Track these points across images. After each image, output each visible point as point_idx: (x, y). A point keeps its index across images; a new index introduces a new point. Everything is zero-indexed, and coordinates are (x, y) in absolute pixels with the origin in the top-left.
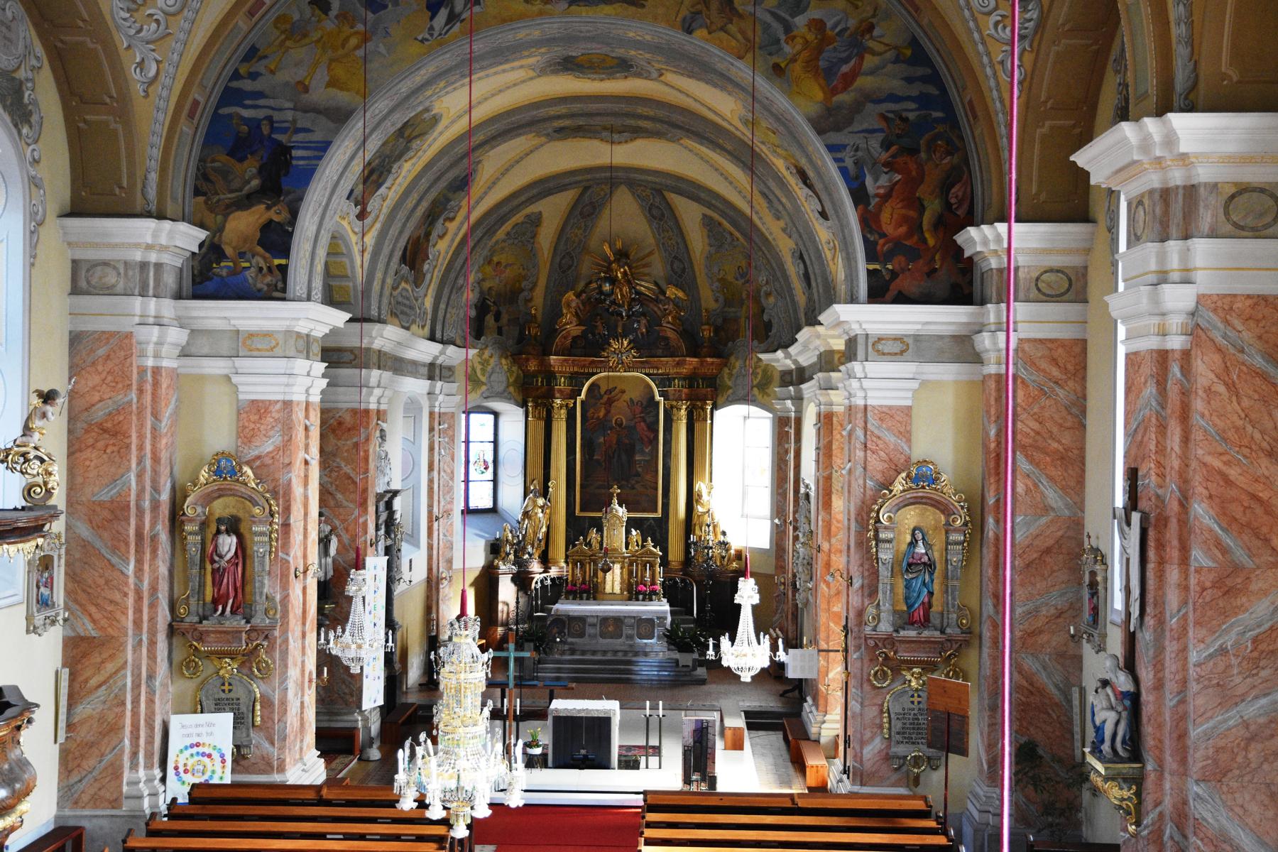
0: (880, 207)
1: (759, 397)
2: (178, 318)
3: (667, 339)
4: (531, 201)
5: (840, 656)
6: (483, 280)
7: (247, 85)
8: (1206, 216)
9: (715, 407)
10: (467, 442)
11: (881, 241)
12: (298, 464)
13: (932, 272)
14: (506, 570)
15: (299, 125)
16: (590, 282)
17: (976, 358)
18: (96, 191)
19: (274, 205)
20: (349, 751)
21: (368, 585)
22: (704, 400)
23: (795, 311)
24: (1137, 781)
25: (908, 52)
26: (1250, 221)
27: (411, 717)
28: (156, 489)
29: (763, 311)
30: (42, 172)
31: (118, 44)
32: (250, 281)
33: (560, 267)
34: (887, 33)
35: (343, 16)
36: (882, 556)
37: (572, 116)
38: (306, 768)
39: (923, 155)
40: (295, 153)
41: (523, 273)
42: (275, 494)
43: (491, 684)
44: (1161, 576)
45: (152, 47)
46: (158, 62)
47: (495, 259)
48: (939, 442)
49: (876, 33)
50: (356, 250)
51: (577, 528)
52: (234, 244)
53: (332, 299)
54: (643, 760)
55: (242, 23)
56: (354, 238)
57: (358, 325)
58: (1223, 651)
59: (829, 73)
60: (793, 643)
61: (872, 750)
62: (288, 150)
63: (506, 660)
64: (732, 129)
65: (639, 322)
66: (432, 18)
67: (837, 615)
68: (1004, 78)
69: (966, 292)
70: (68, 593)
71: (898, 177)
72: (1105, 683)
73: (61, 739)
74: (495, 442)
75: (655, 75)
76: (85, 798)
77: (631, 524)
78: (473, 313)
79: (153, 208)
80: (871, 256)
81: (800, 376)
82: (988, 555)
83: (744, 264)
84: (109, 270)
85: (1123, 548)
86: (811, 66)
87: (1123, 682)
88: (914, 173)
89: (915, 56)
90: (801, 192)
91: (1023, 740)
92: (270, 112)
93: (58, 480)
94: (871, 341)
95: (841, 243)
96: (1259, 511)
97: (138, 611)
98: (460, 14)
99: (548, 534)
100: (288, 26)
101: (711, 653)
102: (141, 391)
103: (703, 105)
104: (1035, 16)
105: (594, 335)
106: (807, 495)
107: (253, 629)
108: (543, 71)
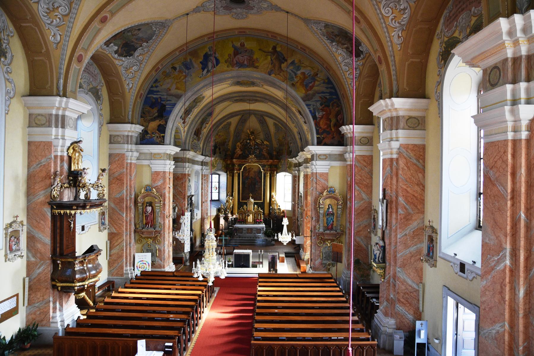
0: (320, 121)
2: (136, 150)
3: (264, 155)
4: (228, 119)
5: (309, 238)
7: (155, 89)
8: (402, 124)
9: (277, 173)
10: (212, 182)
12: (167, 188)
13: (333, 138)
14: (222, 216)
17: (345, 160)
18: (116, 117)
20: (181, 263)
21: (186, 219)
24: (384, 268)
26: (412, 126)
27: (197, 254)
28: (131, 194)
30: (102, 112)
34: (321, 76)
35: (180, 71)
36: (321, 212)
37: (239, 96)
38: (170, 267)
40: (167, 106)
42: (161, 196)
43: (218, 246)
44: (391, 216)
48: (335, 182)
49: (318, 76)
50: (182, 131)
51: (240, 205)
53: (176, 145)
54: (258, 265)
55: (154, 73)
56: (182, 129)
57: (183, 151)
58: (406, 235)
59: (306, 86)
60: (297, 235)
61: (317, 262)
62: (165, 106)
63: (222, 239)
67: (309, 227)
68: (351, 88)
70: (109, 221)
71: (324, 113)
72: (377, 244)
73: (108, 259)
74: (219, 182)
76: (115, 274)
77: (255, 203)
78: (213, 148)
79: (130, 121)
80: (318, 133)
81: (299, 165)
82: (348, 211)
84: (119, 137)
85: (382, 209)
87: (381, 243)
89: (328, 81)
90: (299, 116)
91: (356, 258)
92: (160, 96)
93: (106, 192)
95: (310, 129)
96: (415, 199)
97: (126, 226)
99: (233, 206)
101: (276, 237)
102: (127, 169)
106: (301, 196)
107: (156, 231)
108: (231, 85)
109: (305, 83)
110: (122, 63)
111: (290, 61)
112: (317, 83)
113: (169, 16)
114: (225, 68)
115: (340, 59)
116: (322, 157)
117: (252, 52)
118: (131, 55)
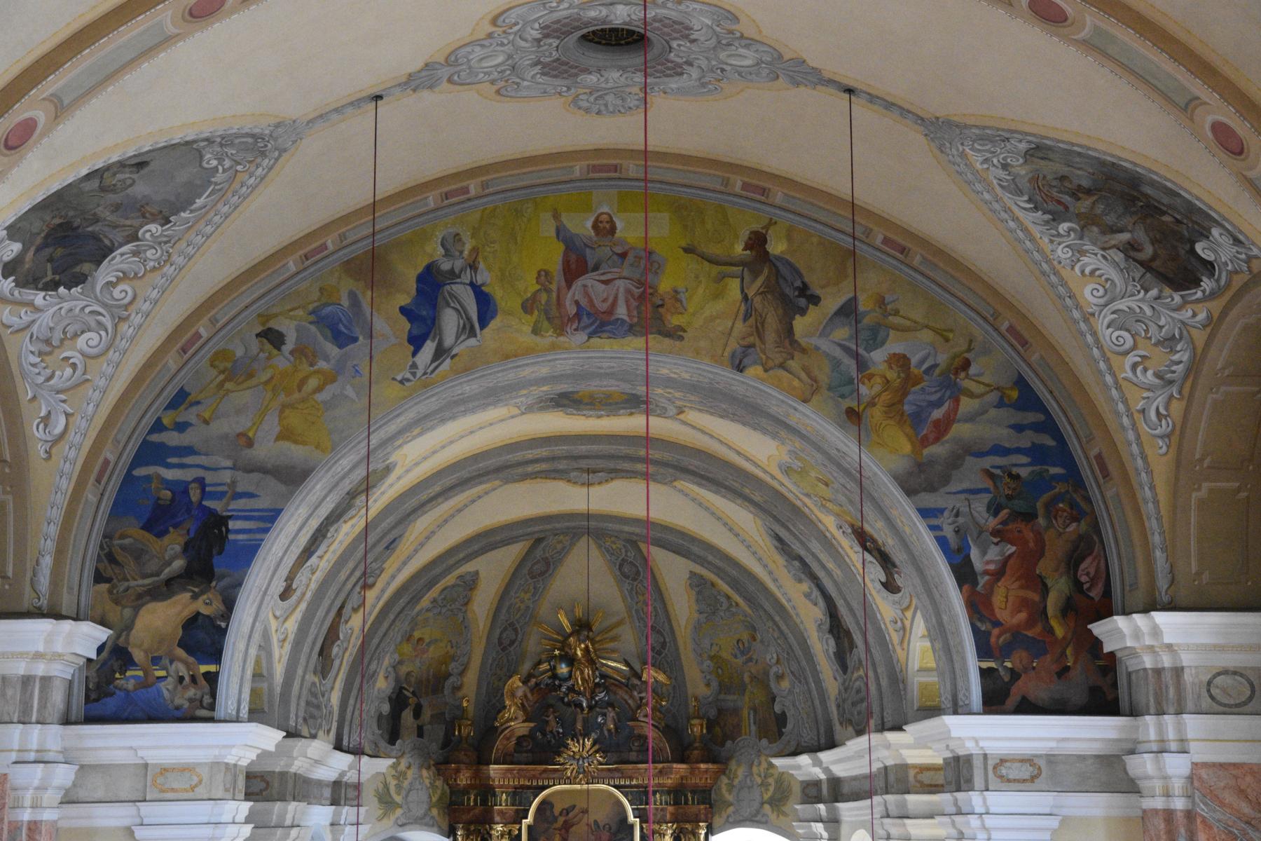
0: (990, 587)
1: (773, 817)
2: (64, 751)
6: (401, 662)
7: (172, 439)
11: (996, 631)
13: (1063, 672)
15: (239, 490)
16: (540, 663)
17: (1131, 787)
19: (202, 593)
22: (696, 821)
23: (823, 701)
25: (1015, 394)
29: (774, 699)
31: (20, 391)
32: (166, 693)
33: (500, 643)
34: (987, 371)
35: (300, 352)
39: (1041, 521)
40: (232, 525)
41: (452, 652)
45: (63, 397)
46: (67, 415)
47: (417, 634)
49: (973, 370)
52: (146, 646)
55: (172, 361)
59: (917, 419)
62: (222, 521)
64: (768, 479)
65: (604, 715)
66: (414, 354)
69: (1110, 697)
75: (672, 411)
78: (386, 708)
80: (984, 650)
83: (745, 636)
86: (894, 409)
88: (1031, 545)
89: (1024, 397)
92: (200, 473)
94: (991, 763)
95: (923, 633)
98: (451, 349)
100: (229, 365)
103: (730, 448)
104: (1185, 358)
105: (544, 734)
108: (530, 409)
109: (907, 408)
110: (26, 319)
111: (832, 302)
112: (966, 405)
113: (295, 107)
114: (524, 335)
115: (1089, 294)
116: (1014, 772)
117: (649, 260)
118: (79, 280)
